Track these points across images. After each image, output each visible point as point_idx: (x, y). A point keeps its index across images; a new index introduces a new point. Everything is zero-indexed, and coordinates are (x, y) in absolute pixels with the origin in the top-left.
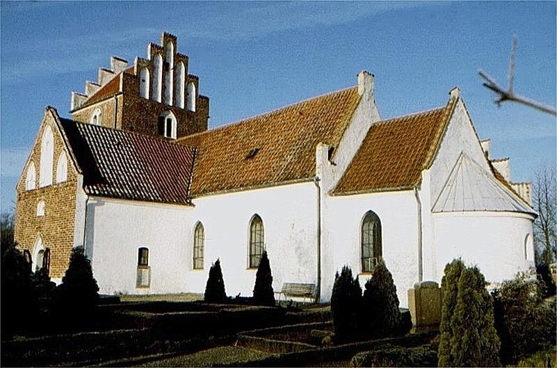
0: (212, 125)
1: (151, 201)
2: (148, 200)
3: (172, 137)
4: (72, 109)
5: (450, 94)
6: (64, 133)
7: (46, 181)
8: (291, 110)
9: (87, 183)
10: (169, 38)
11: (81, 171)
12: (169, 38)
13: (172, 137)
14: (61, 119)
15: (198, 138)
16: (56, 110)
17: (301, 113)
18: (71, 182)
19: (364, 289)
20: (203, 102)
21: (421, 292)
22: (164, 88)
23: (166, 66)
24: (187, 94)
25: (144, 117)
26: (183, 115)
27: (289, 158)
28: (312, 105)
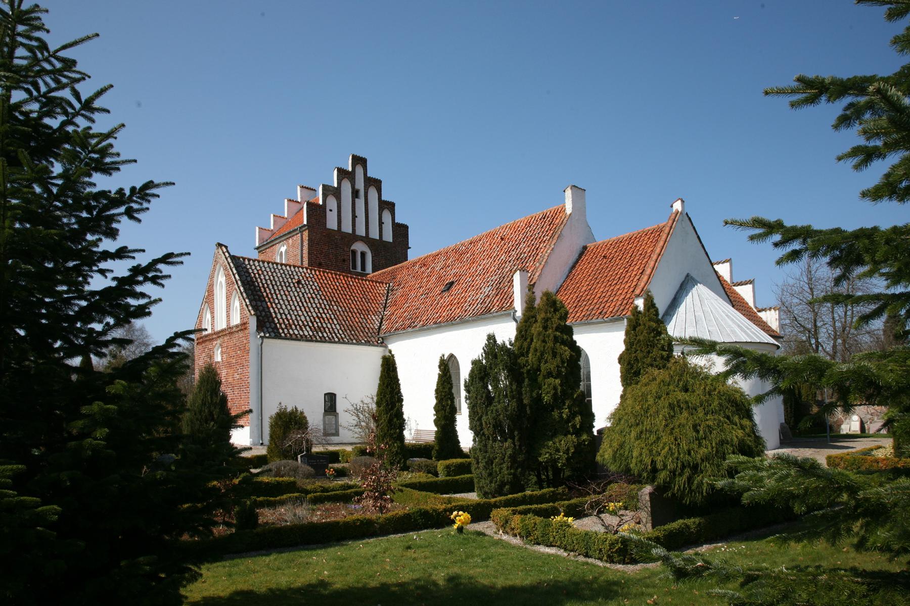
0: (413, 255)
1: (335, 342)
2: (331, 341)
3: (367, 272)
4: (257, 245)
5: (672, 206)
6: (235, 272)
7: (221, 325)
8: (491, 235)
9: (260, 327)
10: (359, 161)
11: (253, 312)
12: (359, 161)
13: (367, 272)
14: (233, 258)
15: (393, 272)
16: (226, 247)
17: (502, 239)
18: (243, 326)
19: (89, 326)
20: (401, 231)
21: (142, 330)
22: (354, 217)
23: (355, 194)
24: (381, 223)
25: (330, 249)
26: (377, 246)
27: (487, 290)
28: (514, 228)
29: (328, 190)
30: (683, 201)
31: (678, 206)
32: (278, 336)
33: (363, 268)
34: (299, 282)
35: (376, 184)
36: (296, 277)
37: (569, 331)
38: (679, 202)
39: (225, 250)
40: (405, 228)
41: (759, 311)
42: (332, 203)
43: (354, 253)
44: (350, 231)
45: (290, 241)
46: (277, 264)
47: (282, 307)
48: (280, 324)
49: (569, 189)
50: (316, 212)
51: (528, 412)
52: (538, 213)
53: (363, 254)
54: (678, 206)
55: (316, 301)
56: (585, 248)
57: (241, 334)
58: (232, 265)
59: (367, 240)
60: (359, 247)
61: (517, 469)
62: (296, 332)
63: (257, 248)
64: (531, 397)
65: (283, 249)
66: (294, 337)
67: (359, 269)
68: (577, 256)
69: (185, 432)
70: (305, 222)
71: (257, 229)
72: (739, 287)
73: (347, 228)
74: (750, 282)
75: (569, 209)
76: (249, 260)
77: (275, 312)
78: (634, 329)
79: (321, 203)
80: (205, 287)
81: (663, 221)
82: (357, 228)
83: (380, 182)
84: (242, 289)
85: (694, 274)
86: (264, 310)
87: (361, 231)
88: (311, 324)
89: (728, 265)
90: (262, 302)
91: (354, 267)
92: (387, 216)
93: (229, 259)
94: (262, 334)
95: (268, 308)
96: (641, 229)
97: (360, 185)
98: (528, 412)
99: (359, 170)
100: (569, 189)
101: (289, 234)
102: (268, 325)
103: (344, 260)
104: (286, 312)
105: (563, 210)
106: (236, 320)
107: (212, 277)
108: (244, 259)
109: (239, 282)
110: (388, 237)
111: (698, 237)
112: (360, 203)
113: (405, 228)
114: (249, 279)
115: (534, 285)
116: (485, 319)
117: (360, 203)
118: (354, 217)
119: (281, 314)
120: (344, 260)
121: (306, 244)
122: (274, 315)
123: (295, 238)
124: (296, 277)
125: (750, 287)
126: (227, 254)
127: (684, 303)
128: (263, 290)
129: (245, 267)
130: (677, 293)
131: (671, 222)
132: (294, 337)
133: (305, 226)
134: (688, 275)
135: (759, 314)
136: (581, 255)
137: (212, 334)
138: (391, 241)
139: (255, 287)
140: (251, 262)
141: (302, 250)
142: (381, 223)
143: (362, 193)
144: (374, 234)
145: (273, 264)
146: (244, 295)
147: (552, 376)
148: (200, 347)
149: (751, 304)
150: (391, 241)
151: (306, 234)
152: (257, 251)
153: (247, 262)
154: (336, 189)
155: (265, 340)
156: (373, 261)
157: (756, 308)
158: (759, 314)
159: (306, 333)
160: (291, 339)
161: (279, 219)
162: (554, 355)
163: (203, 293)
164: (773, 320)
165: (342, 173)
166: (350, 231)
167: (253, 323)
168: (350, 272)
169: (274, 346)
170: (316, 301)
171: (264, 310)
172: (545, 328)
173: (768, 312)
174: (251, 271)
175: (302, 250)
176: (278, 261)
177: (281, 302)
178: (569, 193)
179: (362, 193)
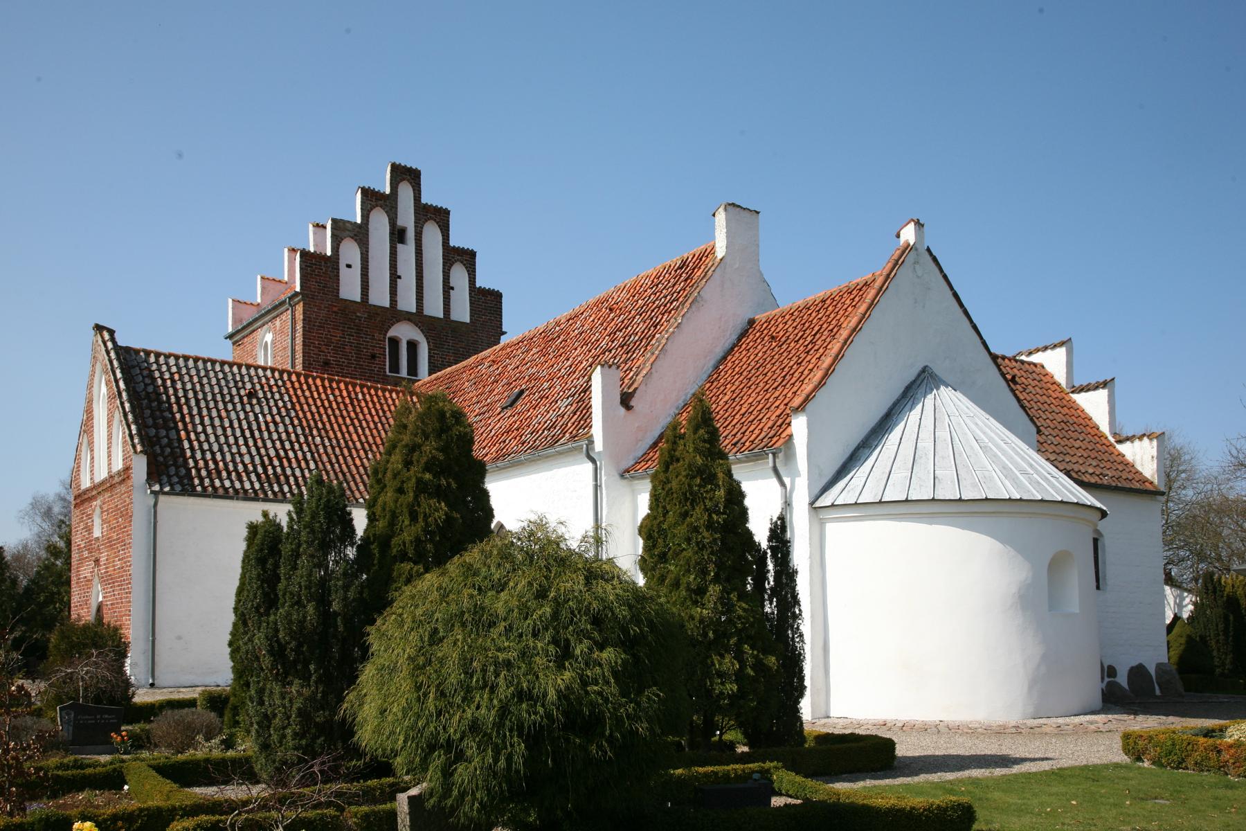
4: (230, 330)
5: (898, 236)
6: (119, 375)
7: (102, 474)
9: (155, 473)
11: (139, 448)
12: (405, 174)
14: (117, 348)
17: (611, 310)
20: (488, 304)
22: (394, 277)
23: (398, 235)
24: (447, 288)
29: (341, 229)
30: (919, 224)
31: (909, 234)
32: (187, 490)
33: (413, 369)
34: (252, 395)
35: (441, 217)
36: (248, 386)
37: (478, 471)
38: (911, 226)
39: (107, 336)
40: (497, 296)
41: (1119, 442)
42: (350, 252)
43: (395, 342)
44: (387, 305)
45: (278, 322)
46: (256, 368)
47: (202, 441)
48: (198, 470)
49: (721, 210)
50: (319, 269)
51: (341, 629)
52: (676, 260)
53: (413, 346)
54: (909, 234)
55: (281, 429)
56: (751, 322)
57: (123, 488)
58: (116, 363)
59: (419, 318)
60: (404, 332)
61: (315, 738)
62: (227, 484)
63: (230, 337)
64: (345, 599)
65: (269, 337)
66: (221, 491)
67: (404, 372)
68: (735, 337)
69: (735, 688)
70: (298, 289)
71: (230, 301)
72: (1083, 394)
73: (380, 297)
74: (1105, 384)
75: (720, 252)
76: (158, 355)
77: (192, 448)
78: (667, 470)
79: (329, 253)
80: (82, 405)
81: (873, 266)
82: (399, 299)
83: (447, 212)
84: (127, 405)
85: (938, 369)
86: (170, 445)
87: (407, 302)
88: (260, 470)
89: (1062, 351)
90: (168, 429)
91: (395, 367)
92: (459, 275)
93: (113, 355)
94: (157, 488)
95: (180, 441)
96: (660, 267)
97: (407, 218)
98: (341, 629)
99: (406, 191)
100: (721, 210)
101: (274, 311)
102: (172, 470)
103: (373, 357)
104: (215, 447)
105: (713, 250)
106: (118, 465)
107: (90, 387)
108: (148, 353)
109: (124, 395)
110: (462, 312)
111: (956, 295)
112: (407, 253)
113: (497, 296)
114: (150, 389)
115: (631, 395)
116: (547, 457)
117: (407, 253)
118: (394, 277)
119: (203, 452)
120: (373, 357)
121: (299, 326)
122: (189, 453)
123: (283, 317)
124: (248, 386)
125: (1103, 394)
126: (110, 345)
127: (903, 424)
128: (175, 408)
129: (148, 368)
130: (895, 405)
131: (890, 265)
132: (221, 491)
133: (296, 294)
134: (924, 370)
135: (1120, 448)
136: (744, 334)
137: (90, 489)
138: (468, 320)
139: (160, 402)
140: (200, 364)
141: (293, 339)
142: (447, 288)
143: (411, 234)
144: (434, 308)
145: (248, 367)
146: (130, 417)
147: (410, 559)
148: (77, 512)
149: (1105, 428)
150: (468, 320)
151: (300, 309)
152: (229, 342)
153: (152, 359)
154: (360, 226)
155: (162, 498)
156: (430, 357)
157: (1115, 435)
158: (1120, 448)
159: (247, 486)
160: (215, 495)
161: (271, 285)
162: (414, 517)
163: (80, 416)
164: (1147, 458)
165: (371, 198)
166: (387, 305)
167: (140, 466)
168: (385, 380)
169: (177, 508)
170: (281, 429)
171: (170, 445)
172: (408, 464)
173: (1137, 442)
174: (157, 374)
175: (293, 339)
176: (262, 363)
177: (209, 430)
178: (721, 217)
179: (411, 234)
